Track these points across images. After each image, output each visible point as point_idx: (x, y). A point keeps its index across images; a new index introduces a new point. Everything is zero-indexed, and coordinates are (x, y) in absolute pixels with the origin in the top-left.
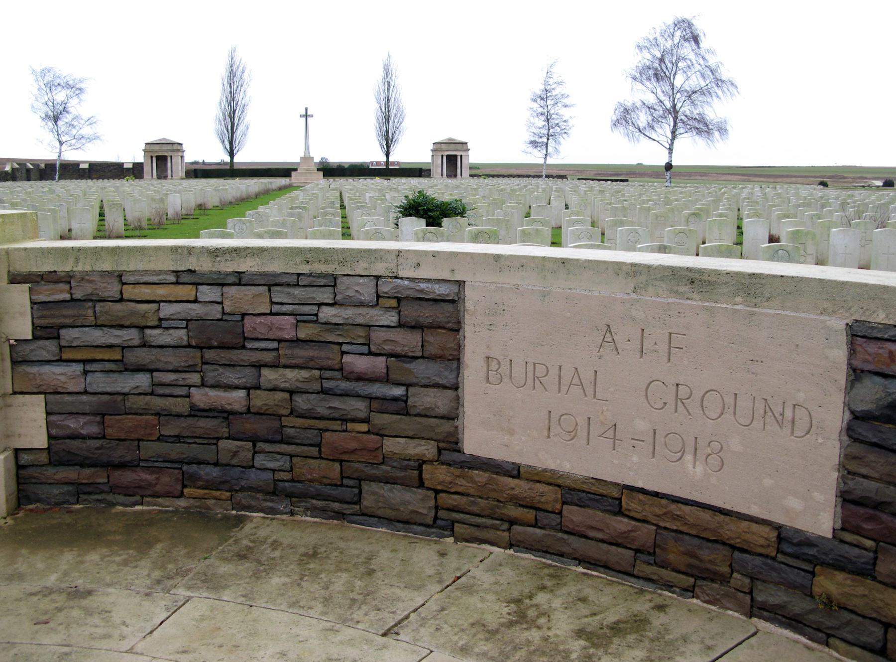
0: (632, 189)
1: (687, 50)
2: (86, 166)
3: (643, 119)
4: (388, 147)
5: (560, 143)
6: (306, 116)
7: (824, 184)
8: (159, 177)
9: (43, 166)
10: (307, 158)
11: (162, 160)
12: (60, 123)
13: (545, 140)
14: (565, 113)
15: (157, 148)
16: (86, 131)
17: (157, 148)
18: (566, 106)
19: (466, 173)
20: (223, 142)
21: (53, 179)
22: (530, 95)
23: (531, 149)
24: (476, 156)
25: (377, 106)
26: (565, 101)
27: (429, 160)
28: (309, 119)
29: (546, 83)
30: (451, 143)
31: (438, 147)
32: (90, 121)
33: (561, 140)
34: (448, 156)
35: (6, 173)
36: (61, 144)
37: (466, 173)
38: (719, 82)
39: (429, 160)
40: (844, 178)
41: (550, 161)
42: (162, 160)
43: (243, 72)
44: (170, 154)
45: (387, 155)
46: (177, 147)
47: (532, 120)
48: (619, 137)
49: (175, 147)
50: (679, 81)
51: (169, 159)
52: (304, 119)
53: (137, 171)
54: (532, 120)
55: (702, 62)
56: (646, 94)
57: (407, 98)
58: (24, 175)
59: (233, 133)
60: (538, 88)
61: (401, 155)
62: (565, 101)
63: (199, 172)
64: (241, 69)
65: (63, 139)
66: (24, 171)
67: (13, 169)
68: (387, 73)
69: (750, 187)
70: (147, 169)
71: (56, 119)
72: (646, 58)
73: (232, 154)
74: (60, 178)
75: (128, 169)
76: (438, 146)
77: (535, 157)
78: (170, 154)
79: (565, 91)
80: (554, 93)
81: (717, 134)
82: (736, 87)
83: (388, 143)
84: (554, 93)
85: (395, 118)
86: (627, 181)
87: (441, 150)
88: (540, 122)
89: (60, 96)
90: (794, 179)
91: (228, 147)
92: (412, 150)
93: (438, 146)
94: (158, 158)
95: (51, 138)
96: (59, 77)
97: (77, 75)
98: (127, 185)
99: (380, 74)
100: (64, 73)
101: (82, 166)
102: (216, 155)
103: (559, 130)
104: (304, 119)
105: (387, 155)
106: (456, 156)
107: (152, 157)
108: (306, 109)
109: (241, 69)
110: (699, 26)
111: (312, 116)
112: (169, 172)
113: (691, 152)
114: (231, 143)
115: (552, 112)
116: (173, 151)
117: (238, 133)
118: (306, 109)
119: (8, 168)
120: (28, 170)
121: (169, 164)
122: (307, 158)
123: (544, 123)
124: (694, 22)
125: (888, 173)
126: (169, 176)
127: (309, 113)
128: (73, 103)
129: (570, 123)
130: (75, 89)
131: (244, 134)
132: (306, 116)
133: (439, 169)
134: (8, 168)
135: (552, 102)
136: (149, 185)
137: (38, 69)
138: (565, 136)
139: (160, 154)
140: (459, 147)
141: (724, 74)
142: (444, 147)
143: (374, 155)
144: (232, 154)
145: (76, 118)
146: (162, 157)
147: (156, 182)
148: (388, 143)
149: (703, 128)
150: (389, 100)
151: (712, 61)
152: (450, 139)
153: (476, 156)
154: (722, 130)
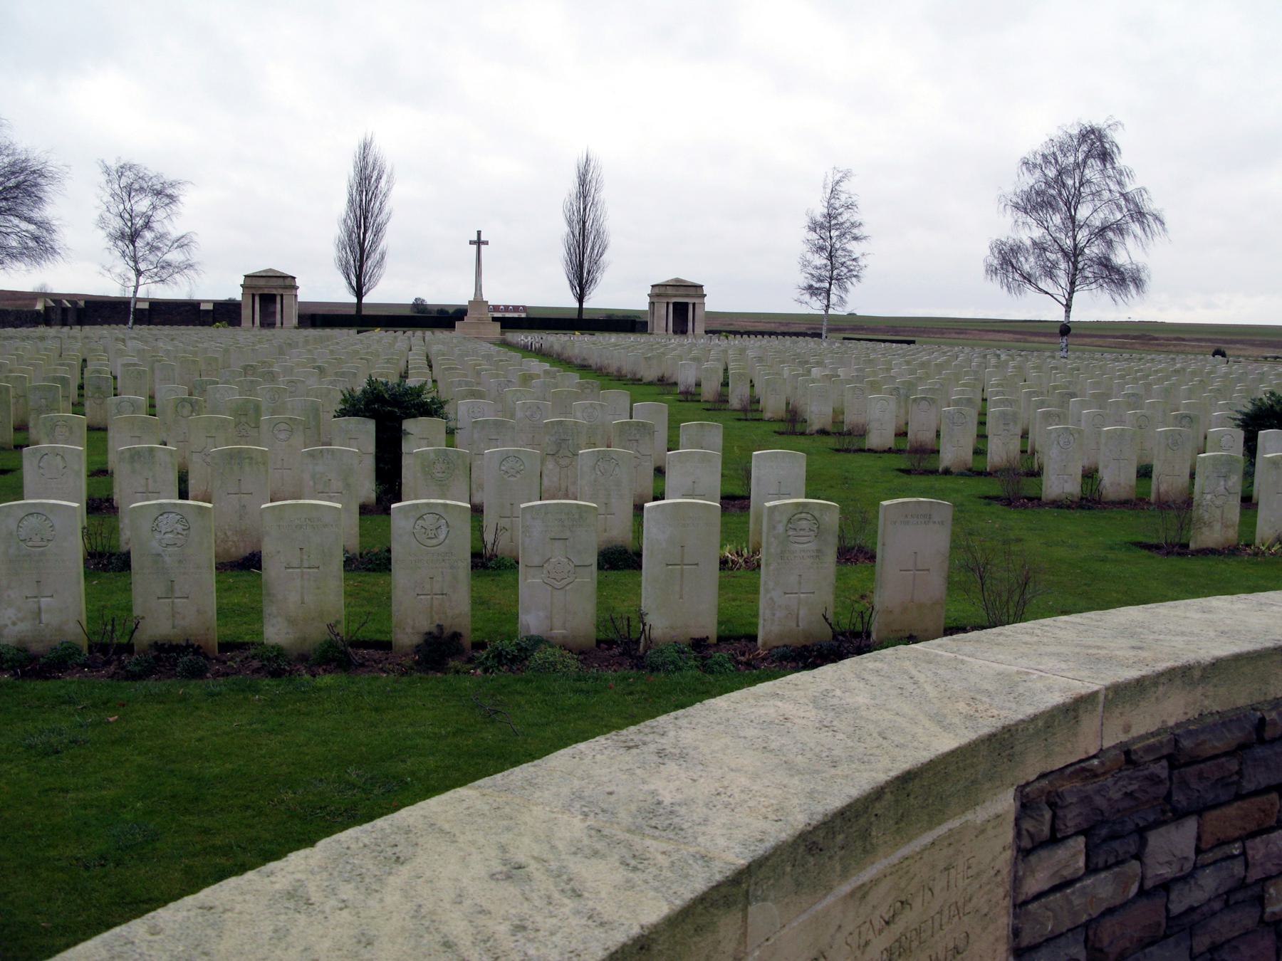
0: (923, 353)
1: (1093, 172)
2: (210, 307)
3: (1029, 264)
4: (582, 289)
5: (846, 290)
6: (479, 242)
7: (1218, 352)
8: (262, 325)
9: (82, 304)
10: (478, 302)
11: (268, 300)
12: (139, 243)
13: (827, 285)
14: (856, 248)
15: (262, 282)
16: (174, 256)
17: (262, 282)
18: (856, 238)
19: (700, 329)
20: (348, 277)
21: (126, 323)
22: (806, 221)
23: (807, 297)
24: (713, 304)
25: (566, 229)
26: (855, 231)
27: (645, 307)
28: (483, 247)
29: (830, 205)
30: (679, 285)
31: (659, 292)
32: (181, 243)
33: (848, 285)
34: (675, 304)
35: (38, 312)
36: (139, 273)
37: (700, 329)
38: (1139, 215)
39: (645, 307)
40: (1156, 339)
41: (831, 311)
42: (268, 300)
43: (379, 178)
44: (281, 291)
45: (581, 300)
46: (288, 283)
47: (809, 256)
48: (995, 287)
49: (288, 282)
50: (1083, 212)
51: (278, 299)
52: (475, 247)
53: (226, 313)
54: (809, 256)
55: (1114, 187)
56: (1029, 232)
57: (615, 219)
58: (59, 317)
59: (361, 267)
60: (819, 210)
61: (601, 299)
62: (855, 231)
63: (320, 318)
64: (376, 173)
65: (142, 266)
66: (59, 312)
67: (46, 308)
68: (583, 181)
69: (967, 350)
70: (246, 312)
71: (133, 237)
72: (1030, 180)
73: (359, 293)
74: (135, 323)
75: (207, 311)
76: (662, 290)
77: (814, 307)
78: (281, 291)
79: (856, 218)
80: (840, 220)
81: (1132, 287)
82: (1162, 223)
83: (581, 283)
84: (840, 220)
85: (593, 249)
86: (913, 342)
87: (667, 296)
88: (820, 260)
89: (142, 204)
90: (1088, 340)
91: (354, 283)
92: (620, 290)
93: (662, 290)
94: (261, 296)
95: (123, 267)
96: (142, 178)
97: (169, 176)
98: (220, 335)
99: (571, 185)
100: (151, 173)
101: (203, 307)
102: (338, 293)
103: (845, 270)
104: (475, 247)
105: (581, 300)
106: (687, 304)
107: (253, 296)
108: (479, 233)
109: (376, 173)
110: (1118, 137)
111: (486, 243)
112: (278, 317)
113: (1095, 306)
114: (359, 277)
115: (838, 245)
116: (286, 287)
117: (369, 263)
118: (479, 233)
119: (39, 306)
120: (65, 310)
121: (278, 306)
122: (478, 302)
123: (825, 261)
124: (1108, 132)
125: (1216, 333)
126: (278, 324)
127: (483, 239)
128: (160, 214)
129: (862, 262)
130: (164, 194)
131: (380, 263)
132: (479, 242)
133: (662, 320)
134: (39, 306)
135: (837, 233)
136: (247, 335)
137: (114, 166)
138: (854, 280)
139: (266, 291)
140: (692, 291)
141: (1150, 206)
142: (670, 291)
143: (561, 297)
144: (359, 293)
145: (161, 237)
146: (268, 293)
147: (256, 330)
148: (581, 283)
149: (1119, 278)
150: (584, 223)
151: (1130, 188)
152: (677, 280)
153: (713, 304)
154: (1138, 282)
